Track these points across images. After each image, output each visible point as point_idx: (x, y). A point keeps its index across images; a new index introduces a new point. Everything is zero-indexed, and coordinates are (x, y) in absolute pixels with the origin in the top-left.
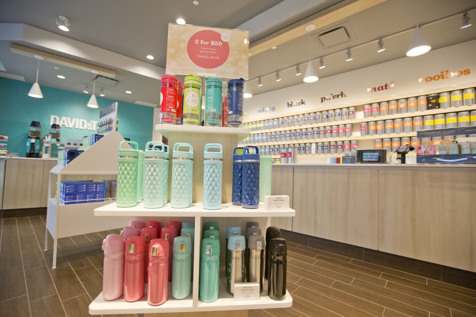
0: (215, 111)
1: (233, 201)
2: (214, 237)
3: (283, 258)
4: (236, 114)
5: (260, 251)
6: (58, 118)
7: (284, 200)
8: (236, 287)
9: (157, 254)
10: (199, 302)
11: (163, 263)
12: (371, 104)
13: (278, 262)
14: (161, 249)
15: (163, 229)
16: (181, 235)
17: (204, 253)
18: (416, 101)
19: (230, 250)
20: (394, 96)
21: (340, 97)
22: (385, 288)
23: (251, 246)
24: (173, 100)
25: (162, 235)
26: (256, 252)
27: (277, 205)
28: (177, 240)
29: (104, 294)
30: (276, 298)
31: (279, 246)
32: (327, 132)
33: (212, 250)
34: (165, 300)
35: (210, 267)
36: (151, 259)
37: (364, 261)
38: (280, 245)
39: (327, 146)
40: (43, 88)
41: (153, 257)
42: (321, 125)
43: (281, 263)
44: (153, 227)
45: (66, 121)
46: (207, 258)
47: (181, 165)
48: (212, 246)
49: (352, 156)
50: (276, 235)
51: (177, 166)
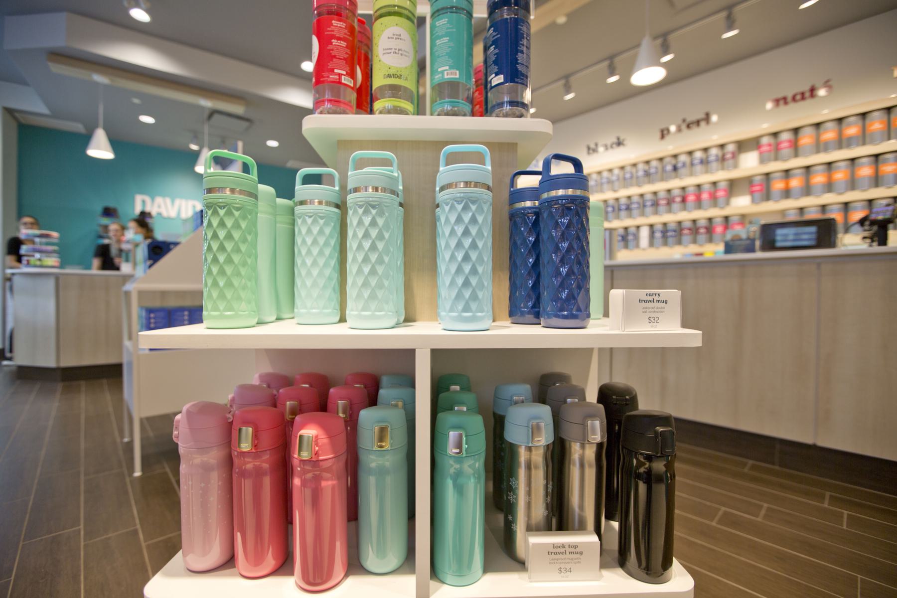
0: (458, 76)
1: (511, 314)
2: (465, 409)
3: (665, 465)
4: (512, 81)
5: (595, 445)
6: (148, 199)
7: (666, 302)
8: (533, 544)
9: (313, 456)
10: (433, 584)
11: (332, 480)
12: (775, 135)
13: (650, 478)
14: (324, 440)
15: (332, 390)
16: (378, 403)
17: (439, 451)
18: (885, 118)
19: (511, 444)
20: (826, 113)
21: (703, 124)
22: (843, 529)
23: (570, 432)
24: (347, 53)
25: (330, 406)
26: (583, 447)
27: (649, 315)
28: (367, 416)
29: (184, 555)
30: (645, 576)
31: (656, 432)
32: (674, 202)
33: (466, 444)
34: (342, 575)
35: (460, 490)
36: (299, 469)
37: (780, 466)
38: (660, 429)
39: (675, 231)
40: (115, 143)
41: (303, 462)
42: (661, 186)
43: (660, 479)
44: (311, 386)
45: (163, 205)
46: (450, 466)
47: (370, 208)
48: (466, 433)
49: (748, 239)
50: (627, 404)
51: (361, 211)
